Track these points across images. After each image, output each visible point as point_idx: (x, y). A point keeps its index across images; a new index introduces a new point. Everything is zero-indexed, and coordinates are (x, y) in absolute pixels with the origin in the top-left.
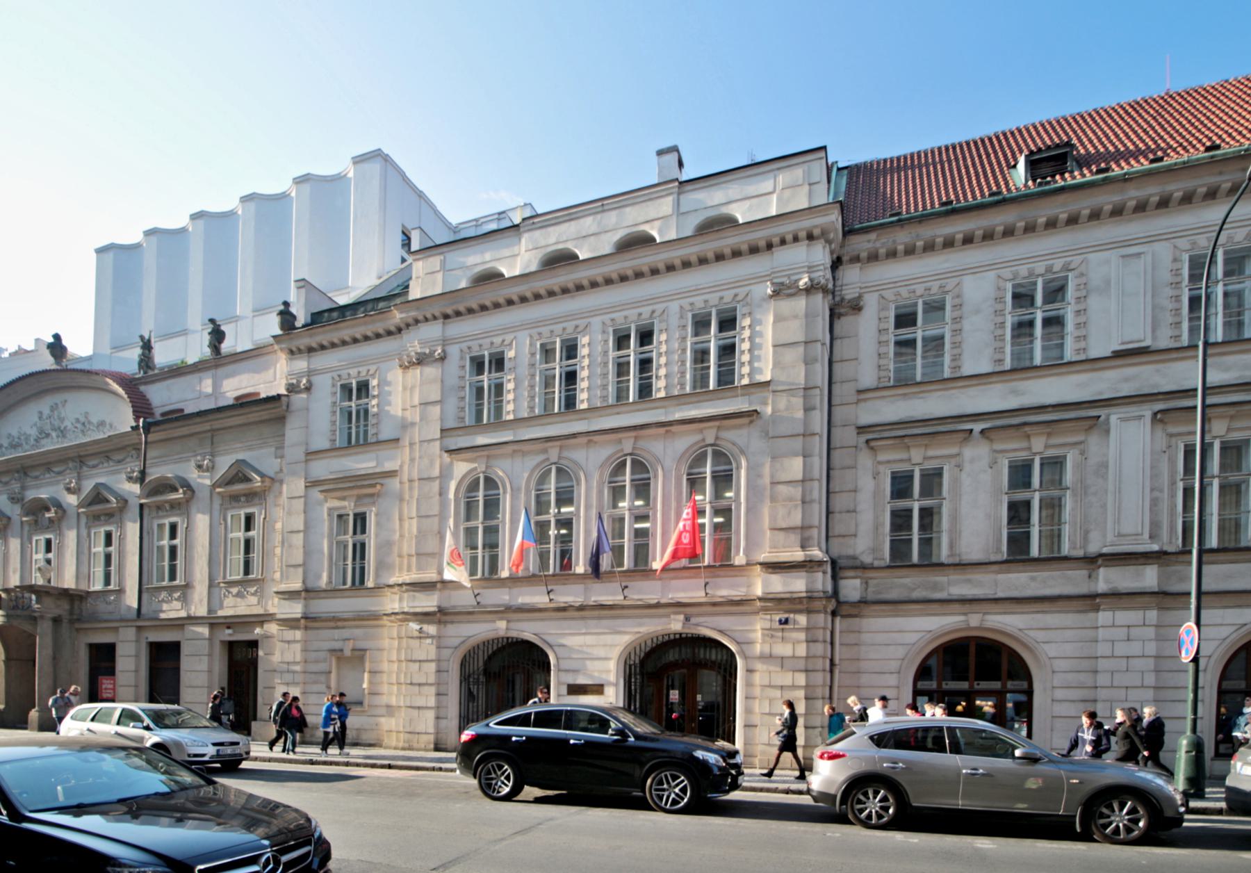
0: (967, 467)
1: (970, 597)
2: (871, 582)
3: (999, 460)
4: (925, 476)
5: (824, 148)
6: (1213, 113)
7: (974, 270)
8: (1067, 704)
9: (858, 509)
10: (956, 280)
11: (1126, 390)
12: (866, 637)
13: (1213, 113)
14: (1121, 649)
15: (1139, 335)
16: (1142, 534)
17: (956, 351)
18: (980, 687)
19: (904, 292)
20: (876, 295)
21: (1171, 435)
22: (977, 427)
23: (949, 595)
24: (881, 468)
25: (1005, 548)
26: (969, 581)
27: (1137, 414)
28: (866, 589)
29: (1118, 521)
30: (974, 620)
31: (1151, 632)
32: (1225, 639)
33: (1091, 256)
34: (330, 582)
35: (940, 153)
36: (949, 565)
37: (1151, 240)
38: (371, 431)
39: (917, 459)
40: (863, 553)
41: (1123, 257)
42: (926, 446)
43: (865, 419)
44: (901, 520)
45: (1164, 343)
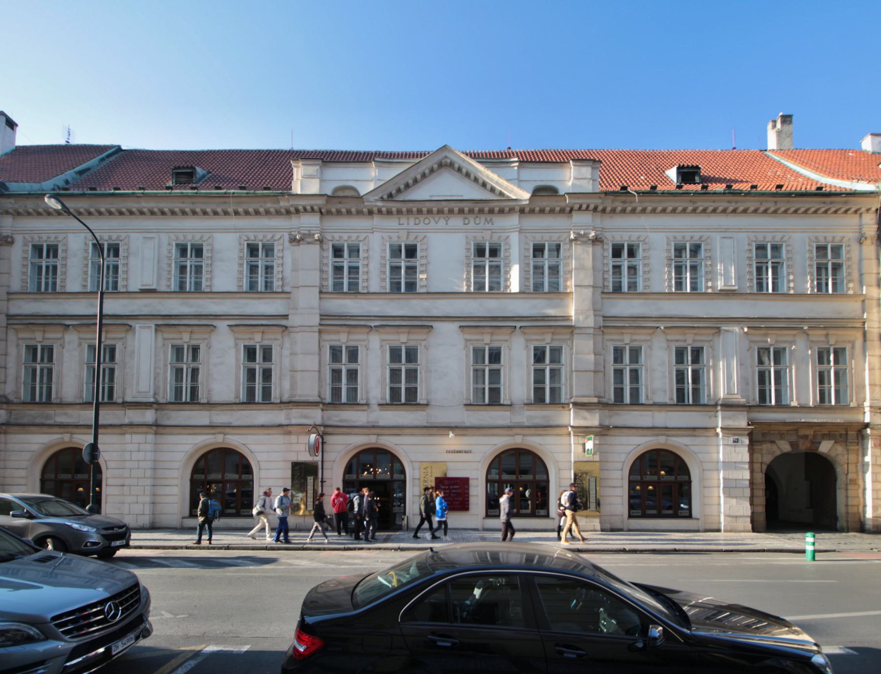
0: (67, 346)
1: (66, 424)
2: (14, 412)
3: (83, 344)
4: (553, 350)
5: (445, 147)
6: (616, 165)
7: (226, 230)
8: (114, 487)
9: (8, 367)
10: (64, 235)
11: (145, 311)
12: (10, 446)
13: (620, 165)
14: (135, 456)
15: (150, 281)
16: (149, 392)
17: (63, 277)
18: (646, 479)
19: (114, 236)
20: (21, 236)
21: (165, 339)
22: (518, 325)
23: (55, 422)
24: (21, 342)
25: (757, 399)
26: (66, 414)
27: (148, 325)
28: (10, 416)
29: (138, 384)
30: (67, 437)
31: (149, 447)
32: (629, 453)
33: (131, 235)
34: (729, 393)
35: (356, 156)
36: (56, 404)
37: (158, 231)
38: (121, 283)
39: (38, 337)
40: (10, 393)
41: (144, 238)
42: (409, 333)
43: (14, 311)
44: (395, 375)
45: (163, 288)
